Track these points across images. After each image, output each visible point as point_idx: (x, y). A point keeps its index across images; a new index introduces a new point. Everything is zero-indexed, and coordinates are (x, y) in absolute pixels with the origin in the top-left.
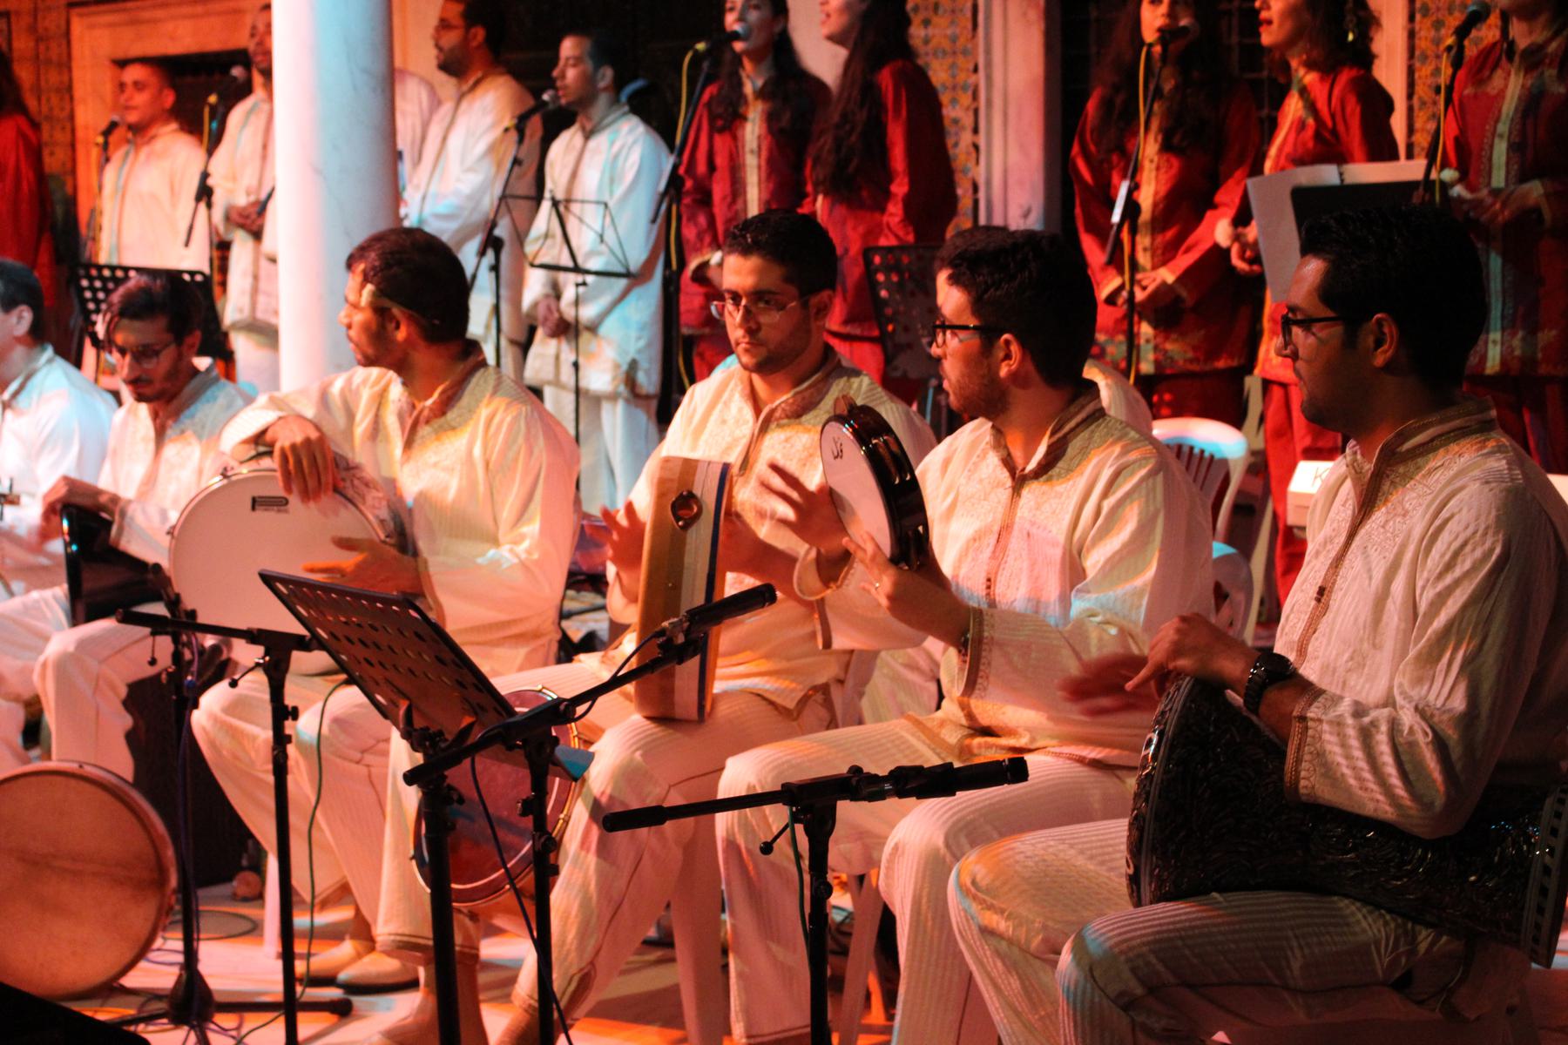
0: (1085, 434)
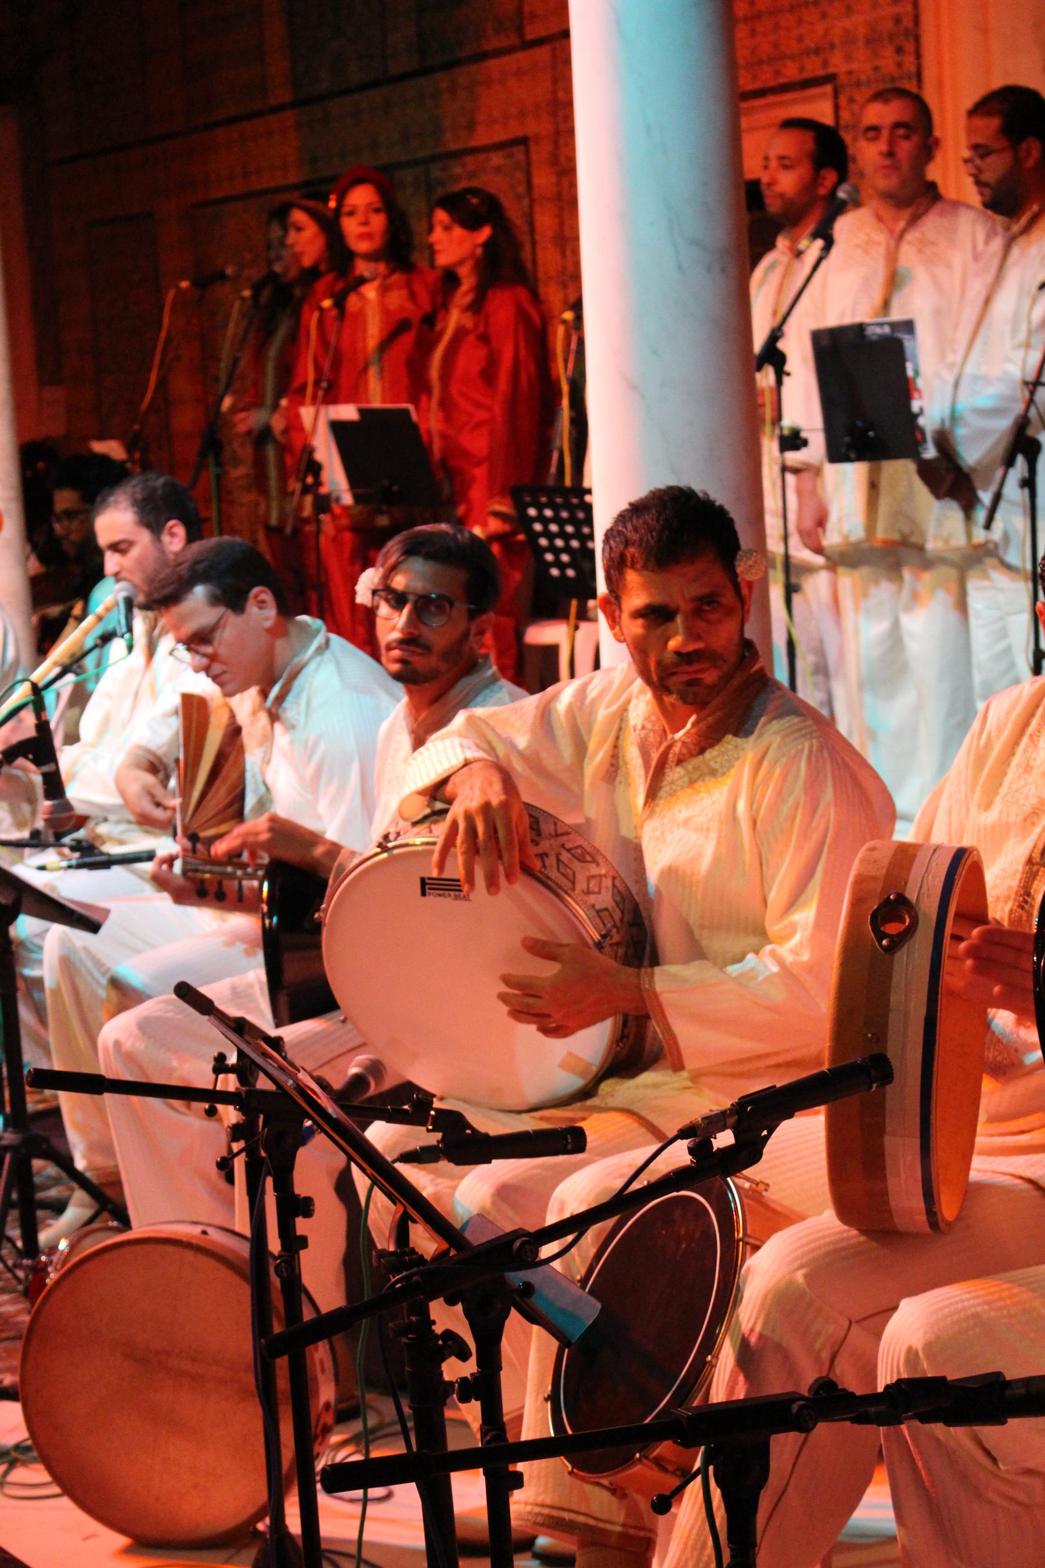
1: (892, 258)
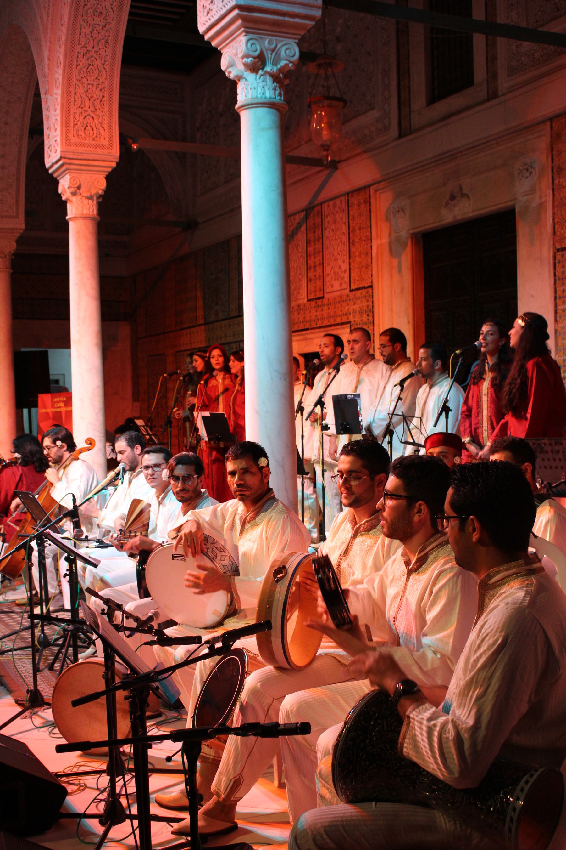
0: (436, 553)
1: (359, 375)
